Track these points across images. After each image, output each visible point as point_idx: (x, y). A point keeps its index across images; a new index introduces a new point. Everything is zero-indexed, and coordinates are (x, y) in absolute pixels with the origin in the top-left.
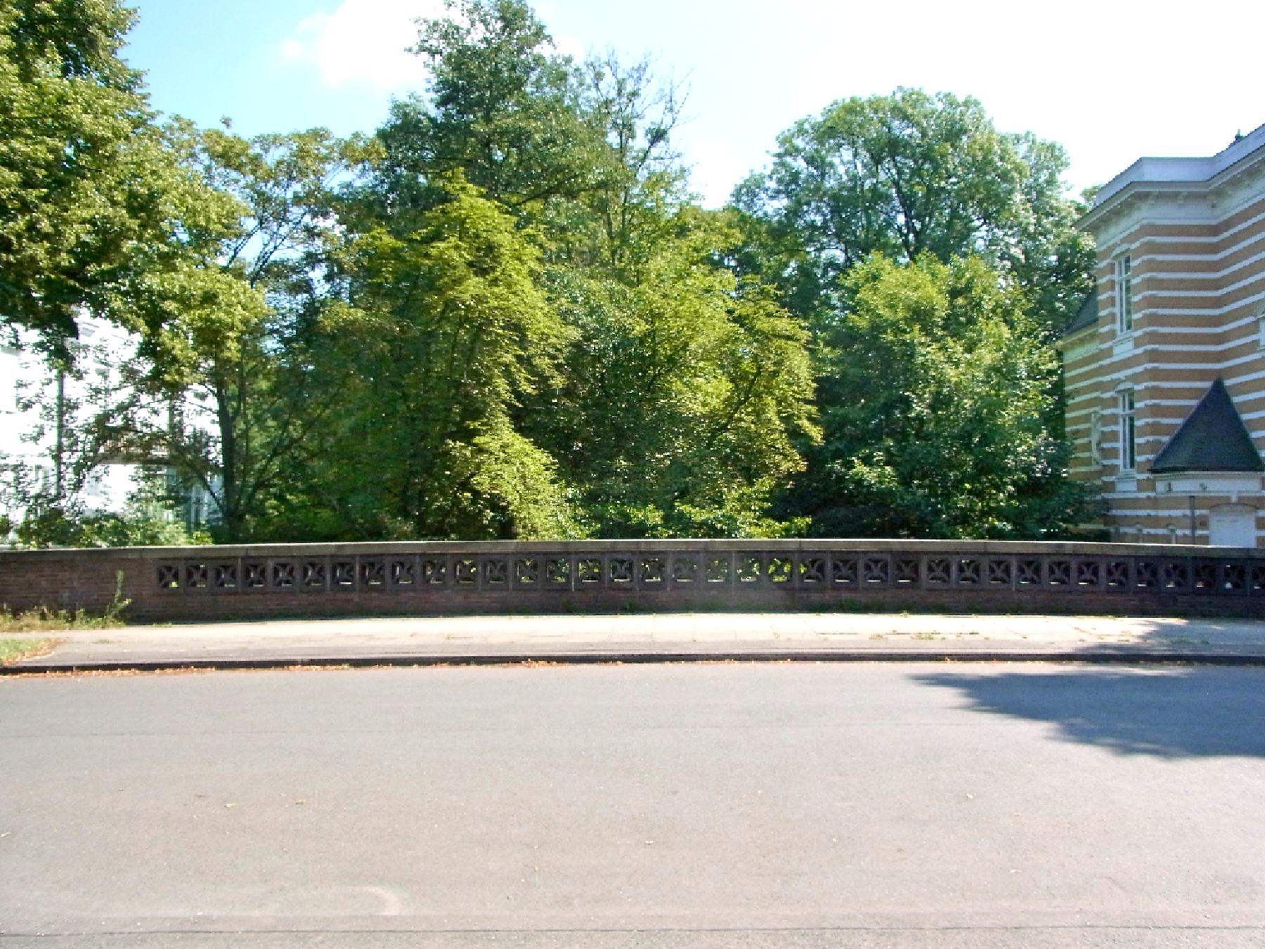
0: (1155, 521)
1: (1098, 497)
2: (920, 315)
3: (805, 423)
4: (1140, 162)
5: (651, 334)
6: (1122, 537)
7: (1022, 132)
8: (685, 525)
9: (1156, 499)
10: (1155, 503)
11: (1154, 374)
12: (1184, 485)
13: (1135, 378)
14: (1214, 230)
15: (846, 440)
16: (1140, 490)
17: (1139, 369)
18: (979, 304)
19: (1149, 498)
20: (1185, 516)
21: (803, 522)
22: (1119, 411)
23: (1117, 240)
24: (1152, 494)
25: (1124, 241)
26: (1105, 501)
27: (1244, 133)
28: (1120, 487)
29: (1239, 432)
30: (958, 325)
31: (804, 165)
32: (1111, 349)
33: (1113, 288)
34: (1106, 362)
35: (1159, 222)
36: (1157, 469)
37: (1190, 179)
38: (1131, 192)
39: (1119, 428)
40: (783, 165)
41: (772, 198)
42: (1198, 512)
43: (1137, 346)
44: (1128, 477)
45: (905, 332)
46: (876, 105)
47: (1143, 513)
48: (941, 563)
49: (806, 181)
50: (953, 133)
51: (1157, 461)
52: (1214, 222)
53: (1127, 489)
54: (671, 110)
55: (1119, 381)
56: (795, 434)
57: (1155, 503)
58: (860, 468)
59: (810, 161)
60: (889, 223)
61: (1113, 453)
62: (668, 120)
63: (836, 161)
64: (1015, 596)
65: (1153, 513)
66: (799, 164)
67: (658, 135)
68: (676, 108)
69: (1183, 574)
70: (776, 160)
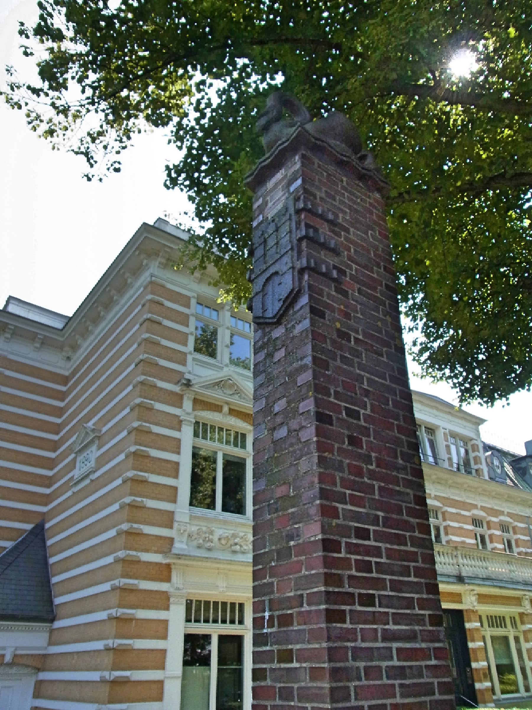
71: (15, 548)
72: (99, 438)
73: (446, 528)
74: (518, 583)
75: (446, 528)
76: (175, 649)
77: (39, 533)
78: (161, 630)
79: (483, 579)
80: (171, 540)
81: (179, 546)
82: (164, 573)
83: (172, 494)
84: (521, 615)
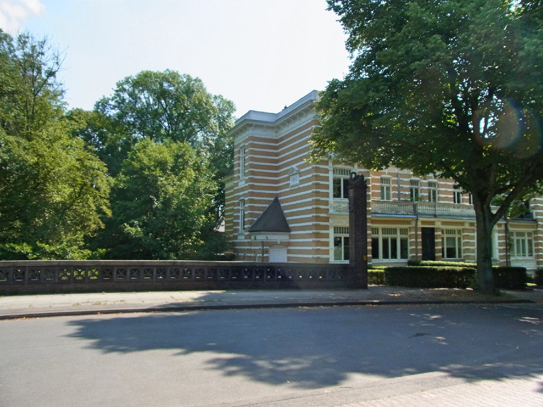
0: (250, 251)
1: (231, 241)
2: (161, 165)
3: (104, 208)
4: (250, 112)
5: (37, 164)
6: (238, 258)
7: (217, 95)
8: (45, 254)
9: (251, 242)
10: (250, 244)
11: (252, 194)
12: (261, 237)
13: (245, 195)
14: (277, 141)
15: (123, 214)
16: (245, 238)
17: (246, 192)
18: (187, 162)
19: (248, 242)
20: (260, 249)
21: (102, 251)
22: (240, 208)
23: (241, 141)
24: (249, 240)
25: (243, 142)
26: (233, 243)
27: (287, 106)
28: (239, 237)
29: (282, 217)
30: (176, 170)
31: (128, 97)
32: (238, 183)
33: (239, 160)
34: (236, 188)
35: (255, 136)
36: (251, 231)
37: (268, 120)
38: (247, 123)
39: (240, 214)
40: (119, 95)
41: (112, 109)
42: (264, 248)
43: (246, 183)
44: (242, 234)
45: (153, 171)
46: (156, 75)
47: (246, 248)
48: (162, 270)
49: (128, 104)
50: (189, 91)
51: (251, 228)
52: (277, 138)
53: (241, 239)
54: (57, 63)
55: (241, 196)
56: (99, 211)
57: (250, 244)
58: (128, 228)
59: (131, 95)
60: (161, 126)
61: (237, 224)
62: (55, 68)
63: (142, 96)
64: (155, 284)
65: (249, 248)
66: (126, 96)
67: (51, 74)
68: (60, 63)
69: (227, 273)
70: (115, 92)
71: (269, 207)
72: (300, 173)
73: (438, 191)
74: (458, 216)
75: (438, 191)
76: (331, 240)
77: (276, 202)
78: (327, 236)
79: (446, 216)
80: (328, 210)
81: (331, 211)
82: (327, 219)
83: (327, 195)
84: (463, 229)
